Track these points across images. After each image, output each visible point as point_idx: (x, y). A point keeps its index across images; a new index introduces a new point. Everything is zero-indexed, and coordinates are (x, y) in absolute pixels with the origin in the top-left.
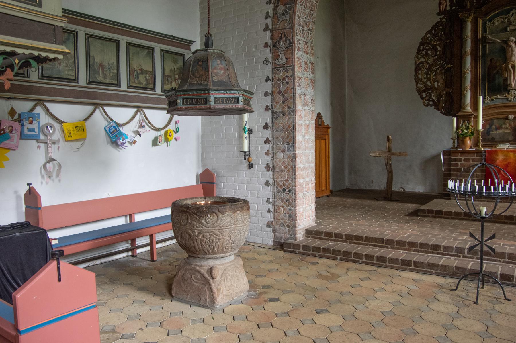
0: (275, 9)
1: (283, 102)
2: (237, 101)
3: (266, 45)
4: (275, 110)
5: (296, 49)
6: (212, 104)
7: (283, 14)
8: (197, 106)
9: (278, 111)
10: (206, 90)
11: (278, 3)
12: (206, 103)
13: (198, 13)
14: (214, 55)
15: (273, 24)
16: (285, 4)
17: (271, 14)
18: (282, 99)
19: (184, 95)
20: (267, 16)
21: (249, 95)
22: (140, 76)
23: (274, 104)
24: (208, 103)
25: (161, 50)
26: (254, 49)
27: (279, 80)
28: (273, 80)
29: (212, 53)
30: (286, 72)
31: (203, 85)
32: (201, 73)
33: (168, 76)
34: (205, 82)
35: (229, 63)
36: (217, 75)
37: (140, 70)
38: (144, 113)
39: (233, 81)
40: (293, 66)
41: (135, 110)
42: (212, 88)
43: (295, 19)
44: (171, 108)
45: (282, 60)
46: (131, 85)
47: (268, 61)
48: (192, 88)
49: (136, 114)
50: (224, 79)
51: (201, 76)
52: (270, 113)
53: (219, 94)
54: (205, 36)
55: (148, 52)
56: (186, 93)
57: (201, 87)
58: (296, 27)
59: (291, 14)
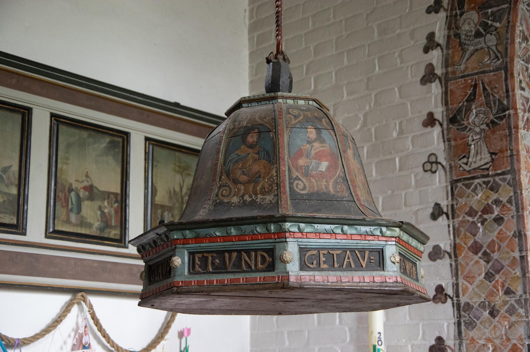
0: (452, 24)
1: (489, 276)
2: (379, 259)
3: (430, 121)
4: (463, 300)
5: (521, 124)
6: (293, 269)
7: (478, 35)
8: (241, 276)
9: (475, 302)
10: (271, 219)
11: (461, 6)
12: (271, 267)
13: (246, 52)
14: (296, 112)
15: (447, 63)
16: (482, 8)
17: (440, 38)
18: (483, 267)
19: (198, 239)
20: (431, 44)
21: (414, 243)
22: (86, 205)
23: (461, 281)
24: (279, 266)
25: (147, 139)
26: (395, 134)
27: (471, 213)
28: (453, 214)
29: (290, 107)
30: (492, 189)
31: (260, 207)
32: (256, 168)
33: (163, 207)
34: (269, 198)
35: (343, 141)
36: (307, 175)
37: (85, 188)
38: (91, 307)
39: (361, 194)
40: (515, 172)
41: (66, 298)
42: (290, 212)
43: (513, 42)
44: (153, 287)
45: (479, 157)
46: (59, 228)
47: (437, 163)
48: (225, 216)
49: (66, 309)
50: (330, 187)
51: (254, 179)
52: (448, 307)
53: (318, 234)
54: (268, 61)
55: (111, 142)
56: (203, 232)
57: (255, 213)
58: (518, 65)
59: (503, 31)
